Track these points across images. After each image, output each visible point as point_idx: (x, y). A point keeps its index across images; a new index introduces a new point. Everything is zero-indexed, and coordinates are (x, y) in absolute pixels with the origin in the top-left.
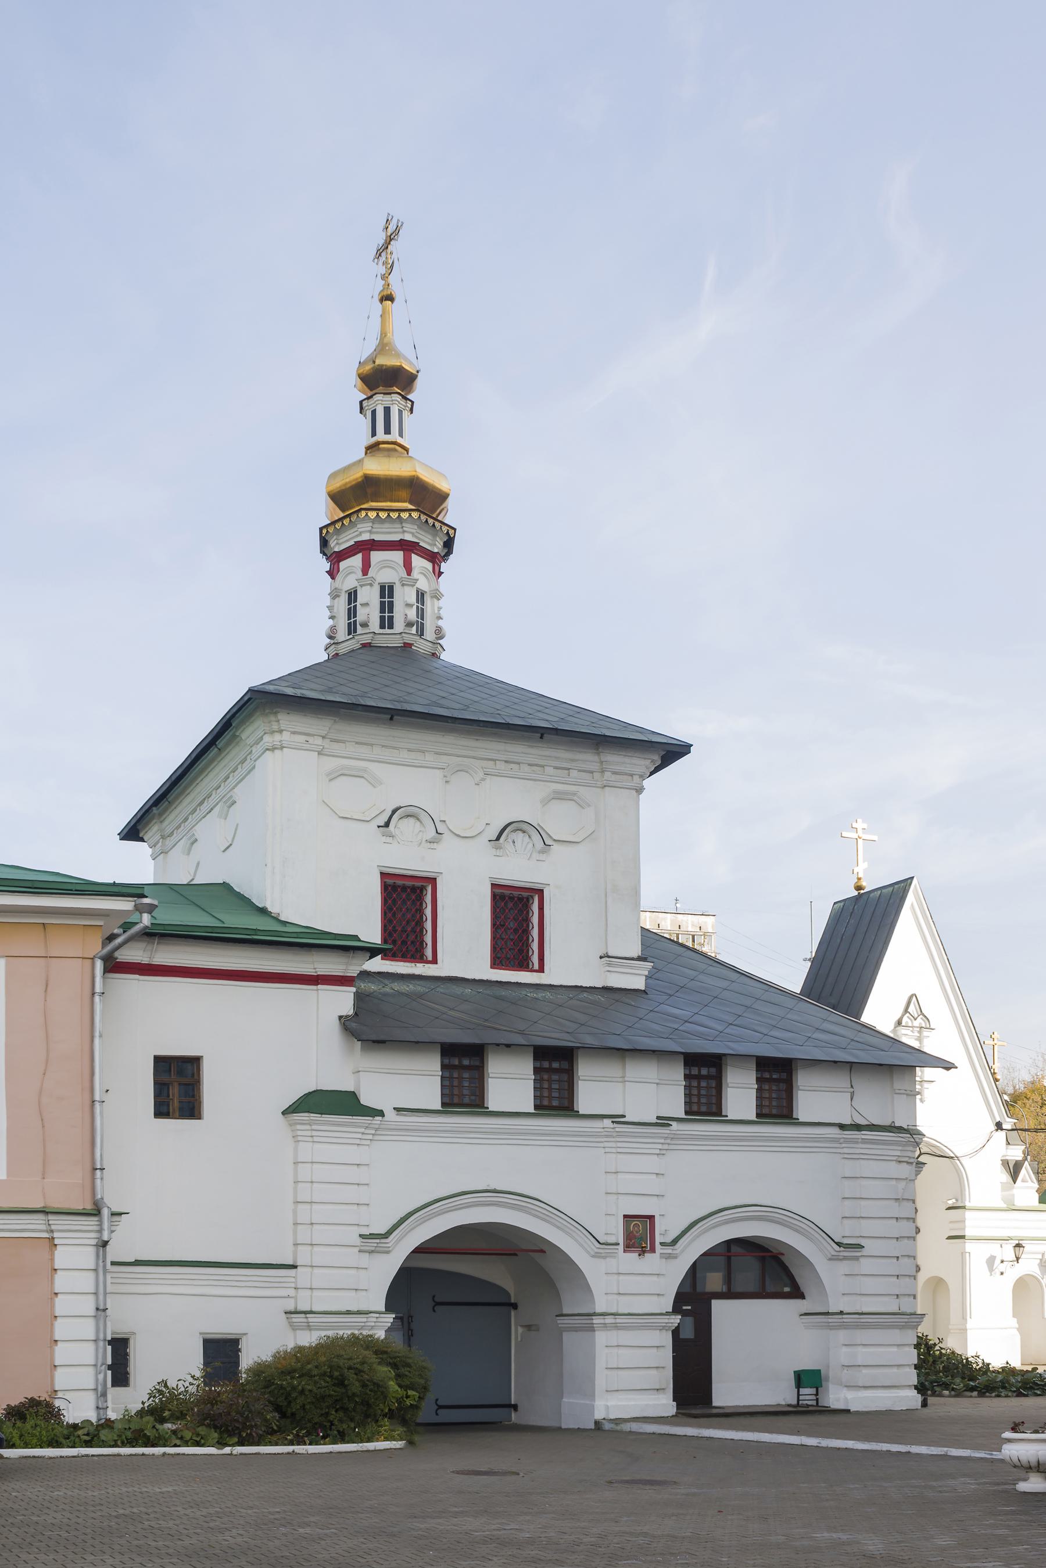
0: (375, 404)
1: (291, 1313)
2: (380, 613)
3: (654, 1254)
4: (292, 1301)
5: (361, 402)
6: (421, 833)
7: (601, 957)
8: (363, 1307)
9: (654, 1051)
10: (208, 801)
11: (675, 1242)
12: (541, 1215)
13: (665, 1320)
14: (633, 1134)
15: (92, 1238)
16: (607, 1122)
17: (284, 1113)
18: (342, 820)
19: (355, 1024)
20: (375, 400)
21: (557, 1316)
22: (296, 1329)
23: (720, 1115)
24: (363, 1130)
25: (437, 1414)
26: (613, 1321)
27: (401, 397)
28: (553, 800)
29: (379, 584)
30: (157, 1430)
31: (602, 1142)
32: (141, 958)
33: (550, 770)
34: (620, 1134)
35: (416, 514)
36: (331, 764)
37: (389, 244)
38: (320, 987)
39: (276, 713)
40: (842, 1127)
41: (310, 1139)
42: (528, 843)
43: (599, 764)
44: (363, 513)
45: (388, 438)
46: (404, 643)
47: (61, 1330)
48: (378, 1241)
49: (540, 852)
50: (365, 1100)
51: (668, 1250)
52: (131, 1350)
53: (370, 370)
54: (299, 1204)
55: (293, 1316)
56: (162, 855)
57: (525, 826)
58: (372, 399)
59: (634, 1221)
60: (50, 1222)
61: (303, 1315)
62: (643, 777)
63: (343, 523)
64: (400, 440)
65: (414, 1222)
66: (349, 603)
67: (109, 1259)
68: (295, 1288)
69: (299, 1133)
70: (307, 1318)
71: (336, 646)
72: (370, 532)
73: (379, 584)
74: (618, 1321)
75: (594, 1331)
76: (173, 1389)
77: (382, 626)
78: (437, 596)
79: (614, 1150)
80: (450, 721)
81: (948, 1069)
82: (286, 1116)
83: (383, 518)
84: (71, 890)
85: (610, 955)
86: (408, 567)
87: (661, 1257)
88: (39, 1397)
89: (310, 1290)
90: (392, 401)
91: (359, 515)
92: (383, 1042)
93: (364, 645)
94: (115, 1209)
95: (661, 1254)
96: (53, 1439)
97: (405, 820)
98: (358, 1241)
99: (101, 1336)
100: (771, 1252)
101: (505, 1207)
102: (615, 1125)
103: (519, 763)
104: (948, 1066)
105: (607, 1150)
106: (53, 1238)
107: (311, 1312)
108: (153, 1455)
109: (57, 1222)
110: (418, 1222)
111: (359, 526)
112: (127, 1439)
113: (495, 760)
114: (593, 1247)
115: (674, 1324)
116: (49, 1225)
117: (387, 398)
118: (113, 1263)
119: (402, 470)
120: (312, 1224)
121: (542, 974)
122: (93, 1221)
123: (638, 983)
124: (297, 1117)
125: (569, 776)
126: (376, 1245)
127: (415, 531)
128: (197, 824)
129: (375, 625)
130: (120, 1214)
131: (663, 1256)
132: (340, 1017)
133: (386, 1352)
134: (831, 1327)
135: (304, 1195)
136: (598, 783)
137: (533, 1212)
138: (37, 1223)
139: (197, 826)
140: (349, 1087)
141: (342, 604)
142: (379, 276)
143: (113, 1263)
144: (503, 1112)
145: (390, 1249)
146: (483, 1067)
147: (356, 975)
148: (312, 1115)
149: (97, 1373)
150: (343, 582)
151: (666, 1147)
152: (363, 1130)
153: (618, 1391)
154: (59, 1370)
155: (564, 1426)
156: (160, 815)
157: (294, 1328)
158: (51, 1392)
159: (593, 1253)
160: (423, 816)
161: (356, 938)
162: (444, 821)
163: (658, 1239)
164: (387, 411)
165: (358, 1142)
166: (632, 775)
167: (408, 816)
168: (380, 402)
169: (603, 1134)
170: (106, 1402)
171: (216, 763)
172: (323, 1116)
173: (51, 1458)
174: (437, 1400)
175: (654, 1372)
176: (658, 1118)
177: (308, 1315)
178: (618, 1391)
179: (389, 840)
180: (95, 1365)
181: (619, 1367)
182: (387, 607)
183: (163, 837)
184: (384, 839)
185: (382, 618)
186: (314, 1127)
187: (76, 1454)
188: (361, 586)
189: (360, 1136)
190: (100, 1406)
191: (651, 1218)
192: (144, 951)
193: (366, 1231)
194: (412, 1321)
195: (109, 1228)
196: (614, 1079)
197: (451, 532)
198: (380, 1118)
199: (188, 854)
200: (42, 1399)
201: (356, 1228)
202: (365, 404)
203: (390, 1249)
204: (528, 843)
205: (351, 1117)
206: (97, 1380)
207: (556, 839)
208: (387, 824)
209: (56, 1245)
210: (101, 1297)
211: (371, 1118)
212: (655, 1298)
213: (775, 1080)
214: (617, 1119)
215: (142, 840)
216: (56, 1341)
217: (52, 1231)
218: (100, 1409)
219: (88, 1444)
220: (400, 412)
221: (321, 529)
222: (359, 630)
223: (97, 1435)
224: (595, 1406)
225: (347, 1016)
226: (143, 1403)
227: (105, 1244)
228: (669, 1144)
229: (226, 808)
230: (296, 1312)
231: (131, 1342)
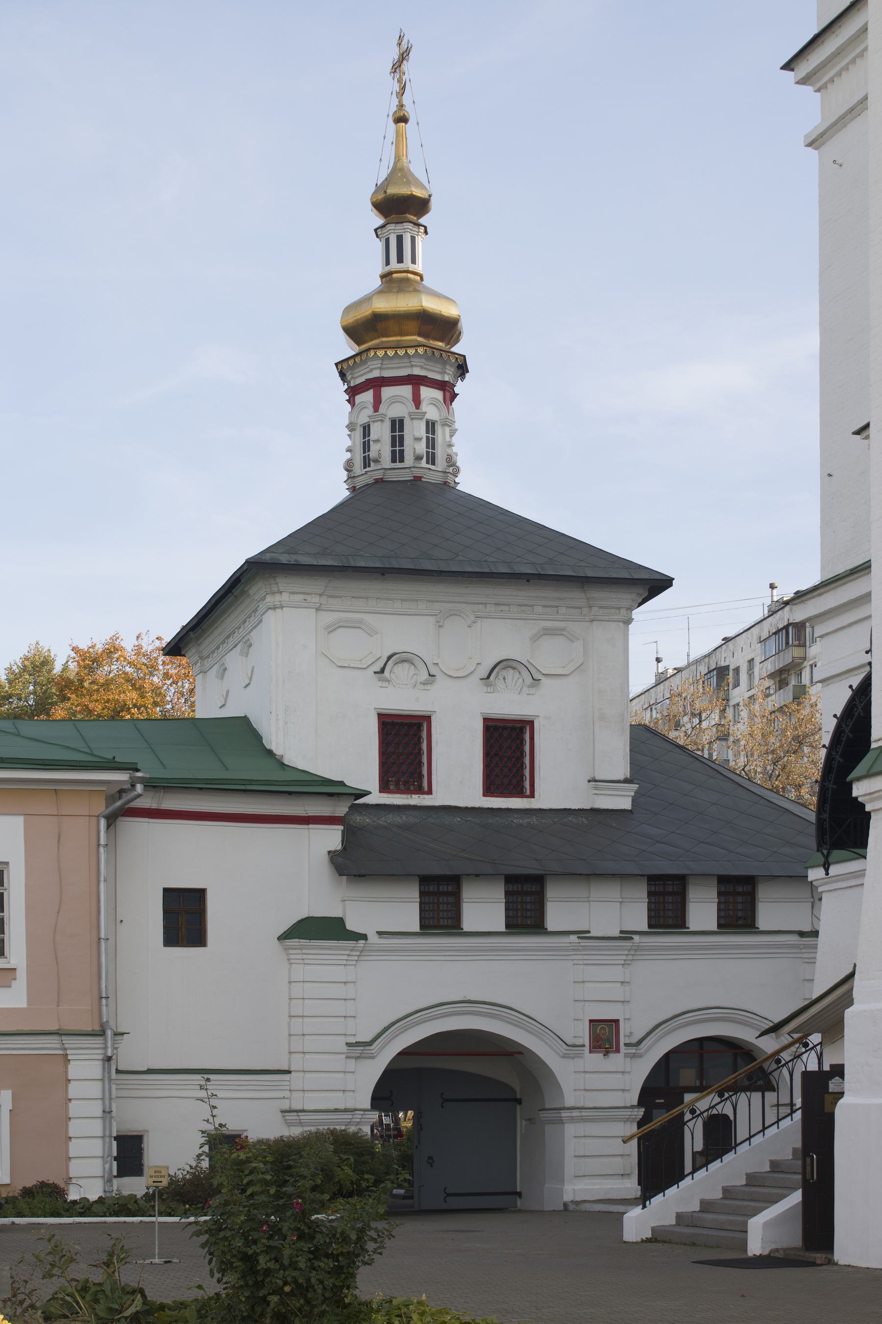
0: (388, 233)
1: (286, 1111)
2: (392, 447)
3: (619, 1054)
4: (288, 1101)
6: (415, 676)
7: (589, 781)
8: (350, 1105)
9: (613, 875)
10: (233, 636)
11: (640, 1042)
12: (512, 1021)
13: (628, 1113)
14: (597, 948)
15: (99, 1054)
16: (573, 938)
17: (279, 938)
18: (339, 669)
19: (341, 859)
20: (388, 229)
21: (539, 1110)
22: (290, 1126)
24: (348, 952)
26: (579, 1114)
27: (412, 225)
28: (544, 636)
29: (390, 418)
30: (138, 1204)
31: (571, 955)
32: (150, 805)
33: (539, 609)
34: (585, 948)
35: (422, 350)
36: (328, 618)
37: (402, 62)
38: (311, 826)
41: (301, 961)
42: (518, 679)
43: (586, 601)
44: (372, 353)
45: (400, 266)
46: (414, 477)
47: (74, 1129)
48: (362, 1048)
49: (529, 687)
50: (350, 926)
51: (632, 1050)
52: (145, 1145)
53: (382, 199)
54: (293, 1018)
55: (286, 1114)
56: (201, 674)
57: (514, 664)
58: (385, 228)
59: (600, 1025)
60: (64, 1042)
61: (295, 1114)
62: (630, 609)
63: (355, 361)
64: (412, 267)
65: (396, 1030)
66: (364, 437)
68: (290, 1090)
69: (292, 957)
70: (299, 1116)
71: (353, 480)
72: (381, 368)
73: (390, 418)
74: (583, 1114)
75: (564, 1123)
76: (172, 1176)
77: (394, 460)
78: (448, 423)
79: (581, 962)
80: (435, 574)
82: (281, 941)
83: (391, 355)
84: (76, 766)
85: (597, 779)
87: (625, 1057)
88: (48, 1180)
89: (302, 1092)
90: (404, 229)
91: (369, 355)
92: (364, 876)
93: (377, 481)
95: (625, 1053)
96: (54, 1211)
98: (345, 1049)
99: (107, 1133)
100: (743, 1049)
101: (481, 1015)
102: (580, 941)
103: (509, 605)
105: (575, 962)
106: (67, 1055)
107: (303, 1111)
108: (133, 1222)
109: (69, 1042)
110: (400, 1031)
111: (369, 363)
112: (114, 1211)
113: (485, 604)
114: (562, 1049)
115: (638, 1117)
116: (63, 1044)
117: (399, 226)
119: (409, 305)
120: (303, 1035)
121: (532, 799)
122: (99, 1041)
123: (625, 804)
124: (289, 942)
125: (558, 613)
126: (360, 1052)
127: (423, 364)
128: (226, 654)
129: (386, 461)
130: (123, 1034)
131: (626, 1055)
132: (329, 852)
133: (351, 1144)
136: (586, 617)
137: (506, 1019)
138: (50, 1045)
139: (227, 656)
142: (394, 93)
144: (476, 932)
145: (375, 1055)
146: (459, 893)
147: (343, 815)
148: (302, 940)
149: (105, 1163)
150: (358, 417)
152: (348, 952)
153: (585, 1176)
154: (73, 1161)
155: (545, 1210)
156: (197, 639)
157: (289, 1124)
158: (67, 1179)
159: (561, 1054)
161: (341, 784)
162: (437, 664)
163: (622, 1040)
164: (400, 239)
165: (345, 962)
166: (619, 608)
167: (403, 661)
168: (393, 231)
169: (570, 948)
170: (112, 1186)
171: (234, 608)
172: (312, 941)
173: (52, 1225)
174: (445, 1188)
175: (619, 1159)
176: (621, 932)
177: (299, 1114)
178: (585, 1176)
179: (385, 684)
180: (103, 1157)
181: (586, 1155)
182: (397, 441)
183: (201, 658)
184: (380, 684)
185: (393, 453)
186: (304, 951)
187: (71, 1222)
188: (374, 422)
189: (346, 957)
190: (107, 1190)
191: (617, 1021)
192: (152, 798)
193: (352, 1040)
194: (421, 1117)
195: (112, 1046)
196: (580, 900)
198: (363, 942)
199: (222, 678)
200: (50, 1182)
201: (343, 1037)
203: (375, 1055)
204: (518, 679)
205: (336, 942)
206: (104, 1168)
207: (545, 673)
208: (382, 671)
209: (69, 1060)
210: (107, 1102)
211: (355, 942)
212: (620, 1093)
213: (739, 894)
214: (582, 934)
216: (70, 1138)
217: (65, 1049)
218: (107, 1192)
219: (81, 1215)
223: (89, 1209)
224: (564, 1190)
225: (335, 851)
226: (148, 1188)
227: (109, 1059)
228: (633, 955)
231: (145, 1139)
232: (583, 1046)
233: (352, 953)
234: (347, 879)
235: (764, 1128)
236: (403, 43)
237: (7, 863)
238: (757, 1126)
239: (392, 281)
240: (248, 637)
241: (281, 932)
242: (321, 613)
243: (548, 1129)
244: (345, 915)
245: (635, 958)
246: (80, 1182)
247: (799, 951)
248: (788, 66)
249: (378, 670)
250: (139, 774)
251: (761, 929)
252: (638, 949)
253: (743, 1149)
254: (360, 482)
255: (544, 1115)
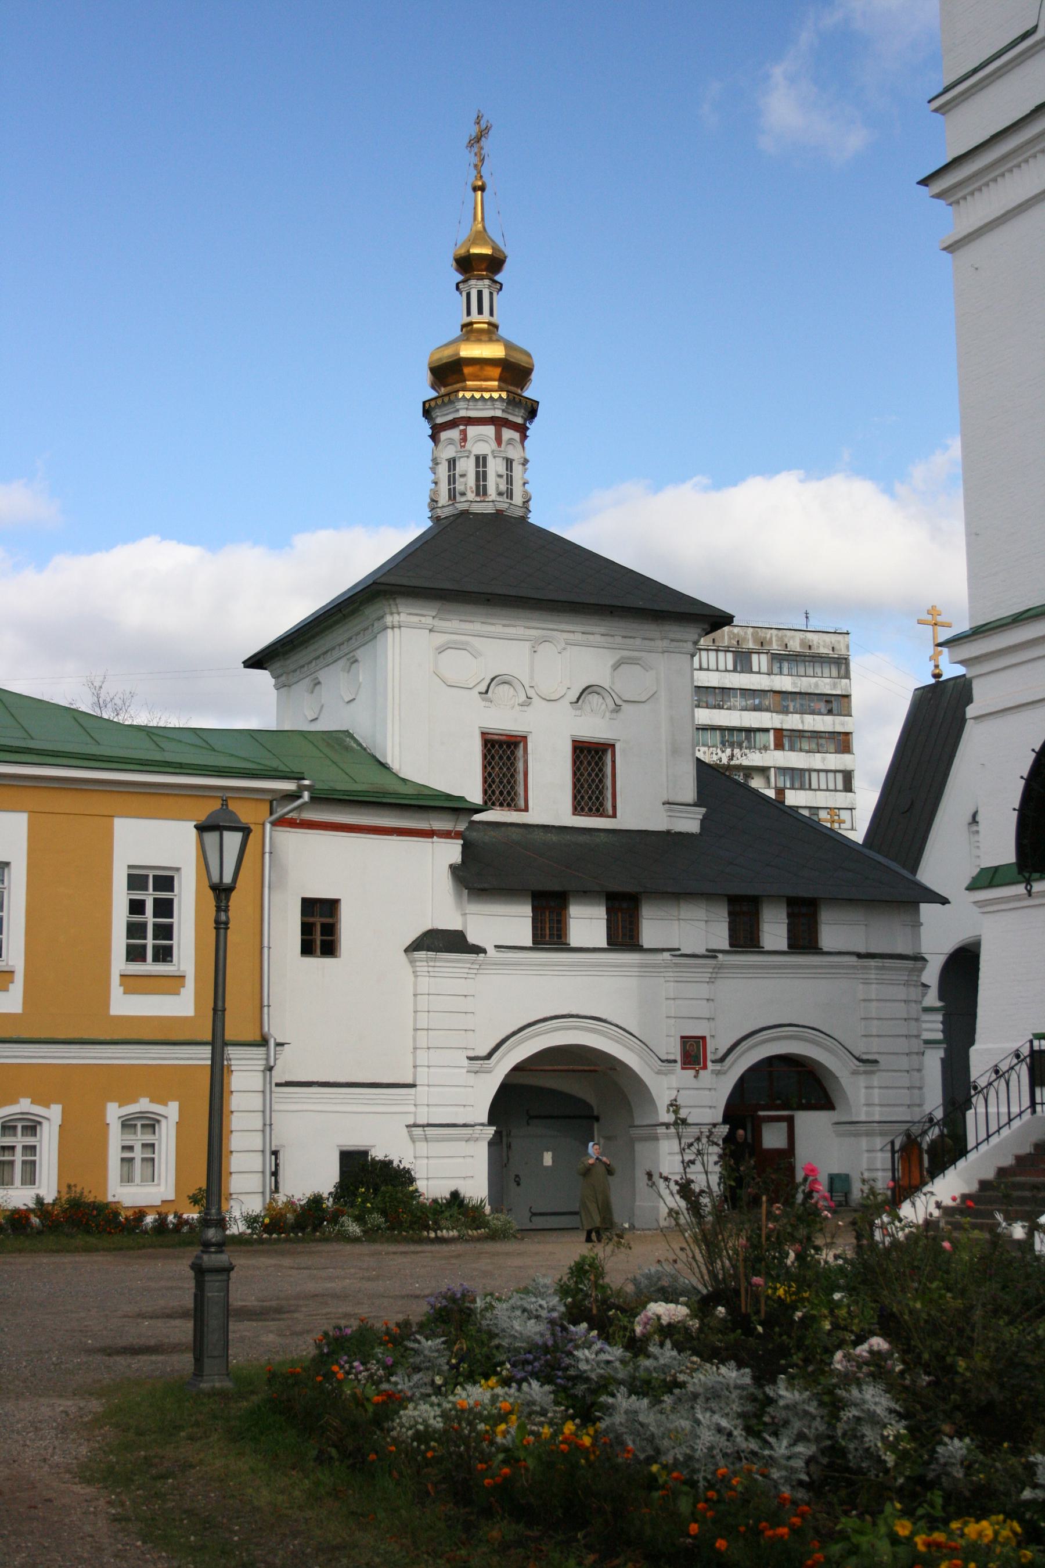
5: (457, 285)
7: (664, 804)
16: (666, 955)
17: (406, 951)
23: (759, 947)
25: (531, 1221)
36: (440, 639)
39: (394, 599)
40: (859, 956)
50: (472, 939)
51: (718, 1067)
61: (421, 1129)
67: (275, 1080)
77: (478, 494)
81: (943, 904)
86: (499, 439)
94: (279, 1040)
97: (501, 686)
98: (466, 1062)
100: (804, 1066)
104: (944, 901)
105: (668, 979)
117: (480, 283)
118: (278, 1085)
122: (262, 1050)
134: (857, 1135)
135: (423, 1021)
140: (458, 927)
141: (443, 470)
142: (472, 165)
143: (278, 1085)
151: (714, 976)
152: (469, 965)
160: (515, 682)
161: (461, 799)
163: (709, 1057)
164: (480, 293)
176: (708, 950)
179: (488, 704)
182: (481, 476)
186: (438, 964)
191: (704, 1038)
193: (472, 1054)
197: (535, 405)
198: (483, 955)
202: (461, 286)
215: (265, 669)
220: (491, 294)
221: (424, 403)
222: (459, 498)
228: (717, 973)
229: (348, 664)
230: (415, 1125)
231: (345, 1149)
232: (675, 1061)
233: (473, 967)
234: (469, 893)
235: (989, 1136)
236: (482, 122)
237: (178, 869)
238: (983, 1135)
239: (472, 331)
240: (354, 653)
241: (408, 942)
242: (432, 633)
243: (639, 1147)
244: (466, 927)
245: (719, 975)
246: (241, 1197)
247: (856, 971)
248: (925, 182)
249: (484, 691)
250: (307, 782)
251: (765, 949)
252: (721, 967)
253: (972, 1156)
254: (443, 513)
255: (634, 1132)
